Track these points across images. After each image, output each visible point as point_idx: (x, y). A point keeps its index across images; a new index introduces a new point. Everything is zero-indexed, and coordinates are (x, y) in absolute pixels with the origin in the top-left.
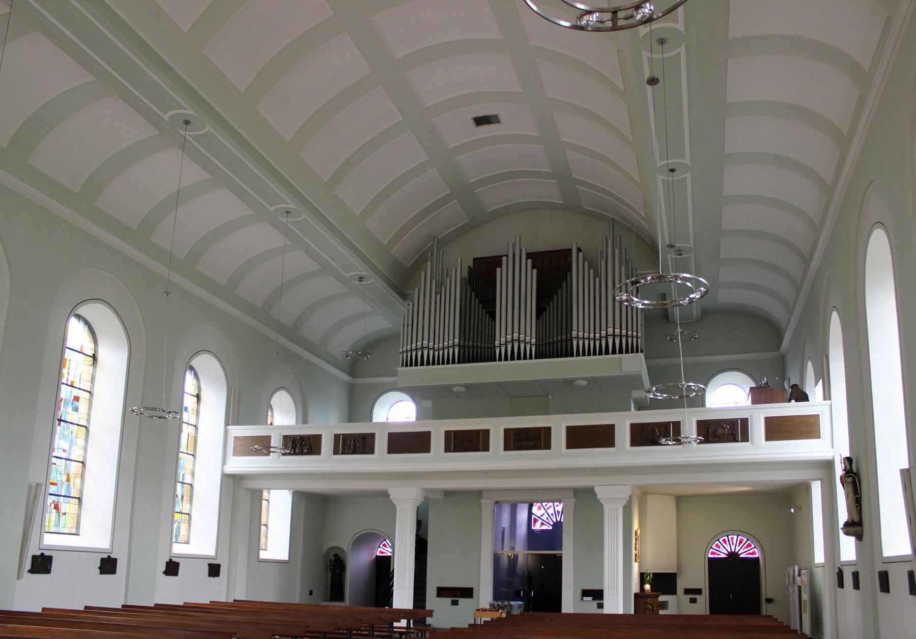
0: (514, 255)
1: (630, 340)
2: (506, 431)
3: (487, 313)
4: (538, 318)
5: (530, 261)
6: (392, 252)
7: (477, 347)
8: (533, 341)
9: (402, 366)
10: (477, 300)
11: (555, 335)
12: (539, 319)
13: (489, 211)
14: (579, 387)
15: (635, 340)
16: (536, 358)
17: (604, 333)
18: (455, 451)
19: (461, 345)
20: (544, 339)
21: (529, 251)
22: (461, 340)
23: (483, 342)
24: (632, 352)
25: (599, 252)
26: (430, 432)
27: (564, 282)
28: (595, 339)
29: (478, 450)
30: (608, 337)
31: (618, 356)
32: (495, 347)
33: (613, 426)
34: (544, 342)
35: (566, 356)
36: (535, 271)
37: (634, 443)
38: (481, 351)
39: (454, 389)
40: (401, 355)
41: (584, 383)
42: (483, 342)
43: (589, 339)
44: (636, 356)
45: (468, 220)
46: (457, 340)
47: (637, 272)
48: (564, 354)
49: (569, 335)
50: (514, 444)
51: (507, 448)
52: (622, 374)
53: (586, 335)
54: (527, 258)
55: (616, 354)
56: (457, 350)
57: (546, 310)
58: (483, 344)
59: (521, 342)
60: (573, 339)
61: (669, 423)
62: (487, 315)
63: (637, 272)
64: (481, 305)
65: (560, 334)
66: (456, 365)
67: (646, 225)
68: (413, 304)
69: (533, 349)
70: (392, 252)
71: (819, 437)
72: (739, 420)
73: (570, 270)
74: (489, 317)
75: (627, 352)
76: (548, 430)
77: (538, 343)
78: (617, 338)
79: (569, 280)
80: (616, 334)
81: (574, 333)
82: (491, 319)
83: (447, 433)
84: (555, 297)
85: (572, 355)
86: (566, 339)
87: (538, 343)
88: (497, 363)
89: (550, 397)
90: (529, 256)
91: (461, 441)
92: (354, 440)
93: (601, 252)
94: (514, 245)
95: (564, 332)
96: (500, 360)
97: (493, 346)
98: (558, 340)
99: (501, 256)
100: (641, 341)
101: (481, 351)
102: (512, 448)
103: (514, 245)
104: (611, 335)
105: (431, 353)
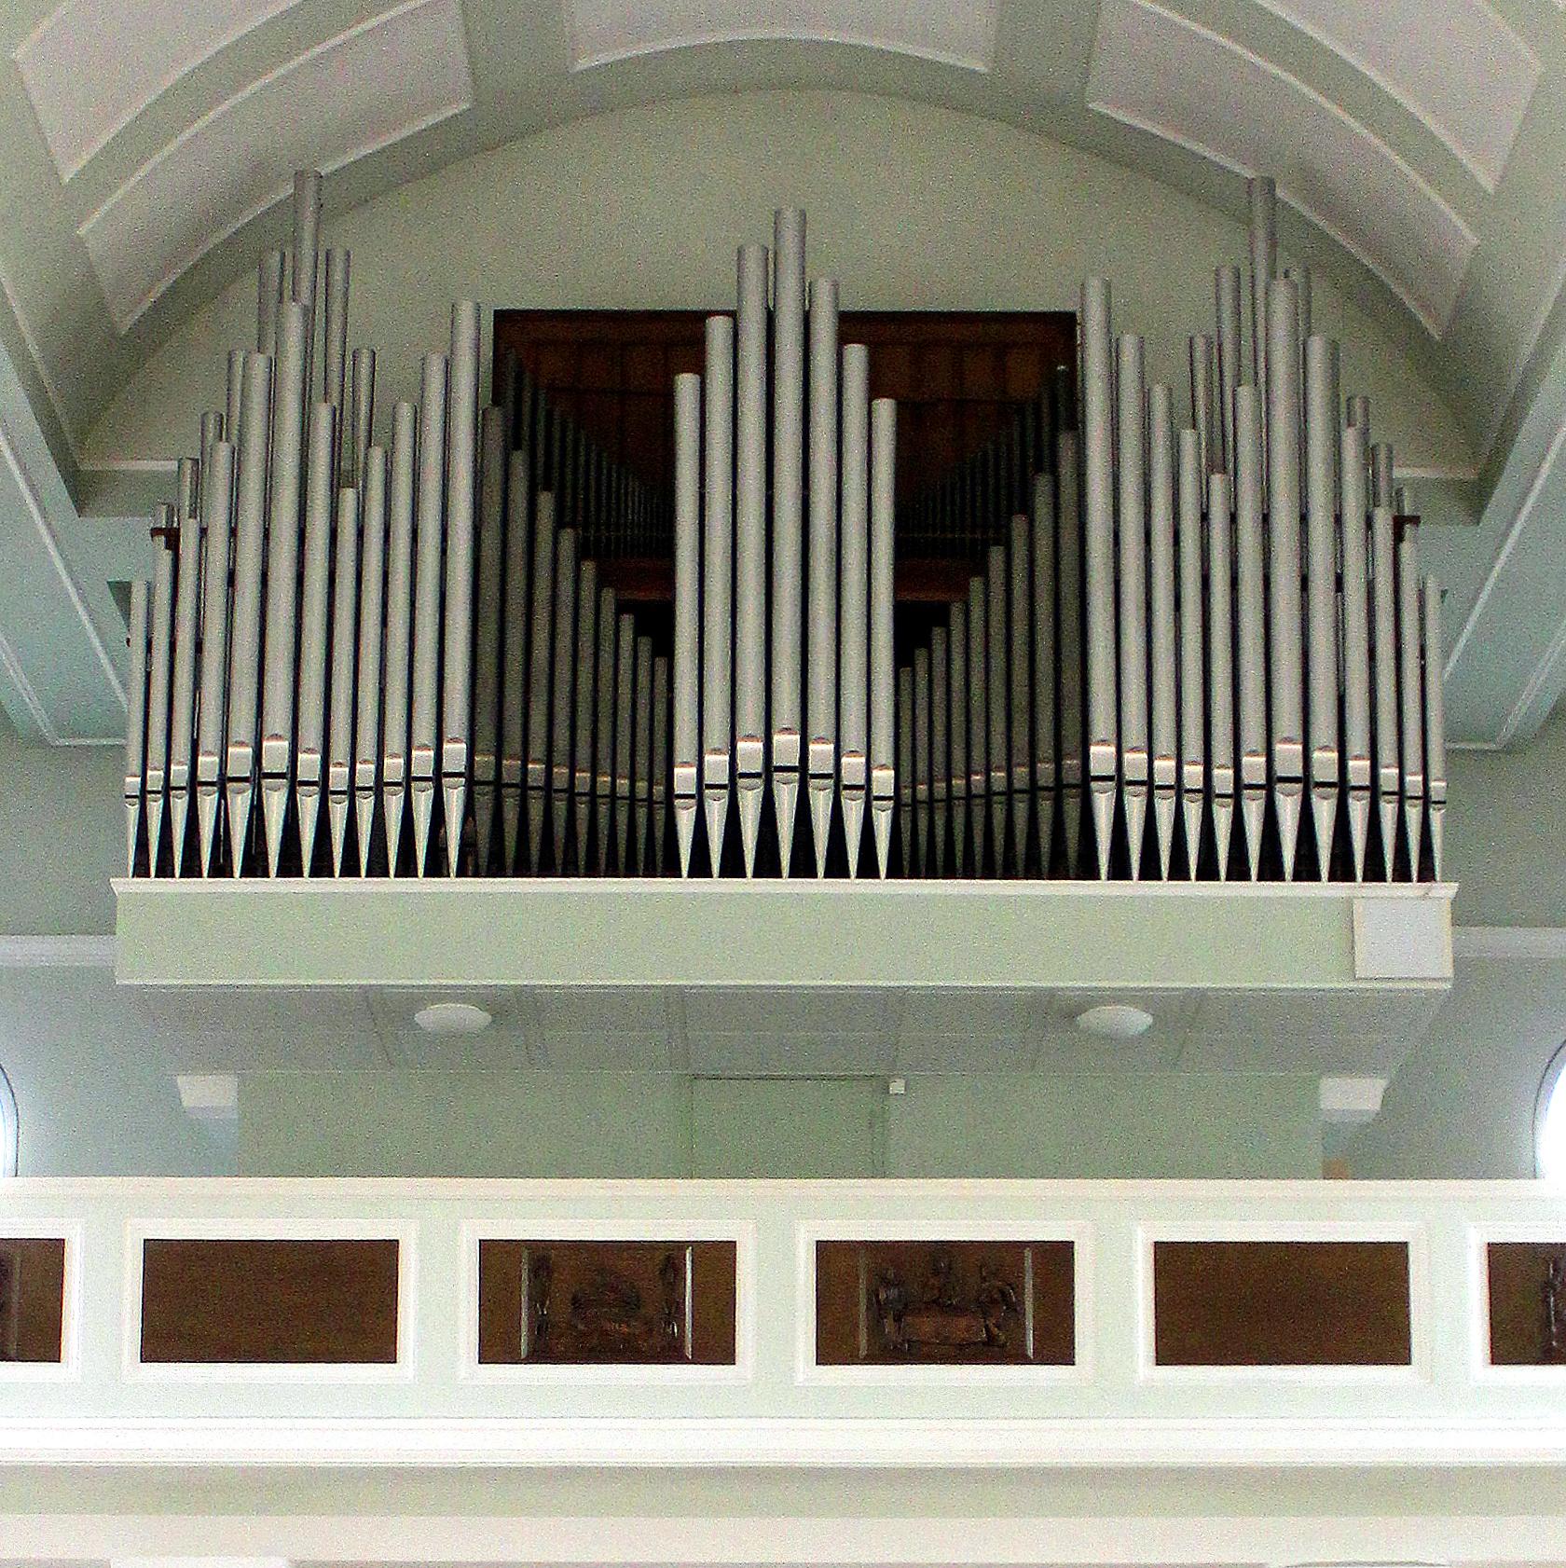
0: (807, 320)
1: (1388, 810)
2: (826, 1251)
3: (621, 608)
4: (903, 658)
5: (856, 355)
6: (82, 231)
7: (593, 794)
8: (884, 780)
9: (141, 870)
10: (567, 538)
11: (998, 755)
12: (912, 664)
13: (583, 64)
14: (1113, 1042)
15: (1413, 814)
16: (894, 872)
17: (1254, 766)
18: (542, 1353)
19: (480, 774)
20: (939, 770)
21: (848, 306)
22: (480, 746)
23: (605, 764)
24: (1402, 875)
25: (1200, 345)
26: (391, 1247)
27: (1042, 485)
28: (1208, 793)
29: (670, 1353)
30: (777, 776)
31: (1324, 889)
32: (670, 794)
33: (1398, 1251)
34: (940, 787)
35: (1057, 872)
36: (885, 408)
37: (1172, 1349)
38: (257, 811)
39: (419, 1017)
40: (133, 811)
41: (1139, 1020)
42: (605, 764)
43: (1179, 789)
44: (1424, 897)
45: (465, 106)
46: (455, 753)
47: (1397, 473)
48: (959, 862)
49: (1072, 763)
50: (875, 1328)
51: (832, 1349)
52: (1352, 985)
53: (179, 774)
54: (843, 339)
55: (300, 875)
56: (455, 799)
57: (945, 623)
58: (605, 779)
59: (300, 789)
60: (1094, 785)
61: (680, 1246)
62: (627, 622)
63: (1397, 473)
64: (588, 568)
65: (1021, 755)
66: (452, 885)
67: (1466, 232)
68: (203, 532)
69: (883, 822)
70: (82, 231)
71: (1406, 1361)
72: (688, 1252)
73: (1075, 421)
74: (638, 632)
75: (1374, 872)
76: (380, 1259)
77: (906, 792)
78: (240, 792)
79: (1066, 470)
80: (506, 779)
81: (1102, 755)
82: (645, 645)
83: (493, 1255)
84: (996, 556)
85: (672, 870)
86: (1059, 788)
87: (906, 792)
88: (1103, 887)
89: (897, 1087)
90: (852, 326)
91: (575, 1300)
92: (1555, 1263)
93: (1209, 343)
94: (771, 263)
95: (1045, 748)
96: (700, 868)
97: (659, 790)
98: (1017, 785)
99: (700, 318)
100: (1445, 817)
101: (257, 811)
102: (863, 1353)
103: (771, 263)
104: (212, 784)
105: (309, 806)
